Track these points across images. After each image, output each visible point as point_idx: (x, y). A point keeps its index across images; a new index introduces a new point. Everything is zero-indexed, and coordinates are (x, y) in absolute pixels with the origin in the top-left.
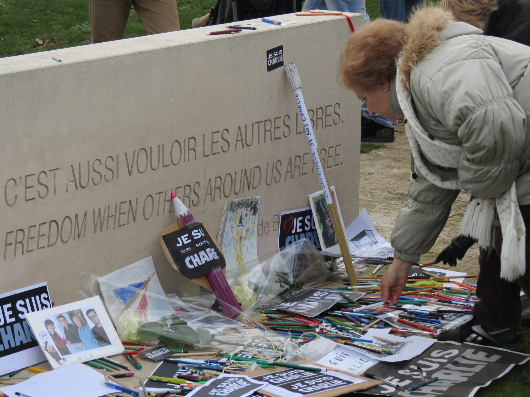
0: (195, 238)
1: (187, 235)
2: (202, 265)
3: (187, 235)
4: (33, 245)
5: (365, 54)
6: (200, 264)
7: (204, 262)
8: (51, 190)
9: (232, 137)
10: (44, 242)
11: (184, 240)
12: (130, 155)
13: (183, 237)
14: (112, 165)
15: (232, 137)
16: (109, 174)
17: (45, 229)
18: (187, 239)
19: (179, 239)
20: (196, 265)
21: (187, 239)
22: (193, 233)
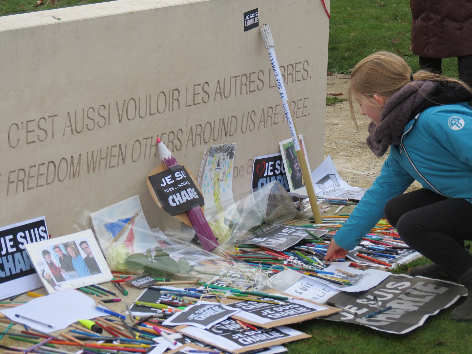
0: (177, 179)
1: (170, 176)
2: (184, 203)
3: (170, 176)
5: (189, 316)
6: (182, 202)
7: (185, 201)
11: (168, 181)
13: (166, 178)
18: (170, 179)
19: (163, 180)
20: (178, 203)
21: (170, 179)
22: (176, 175)
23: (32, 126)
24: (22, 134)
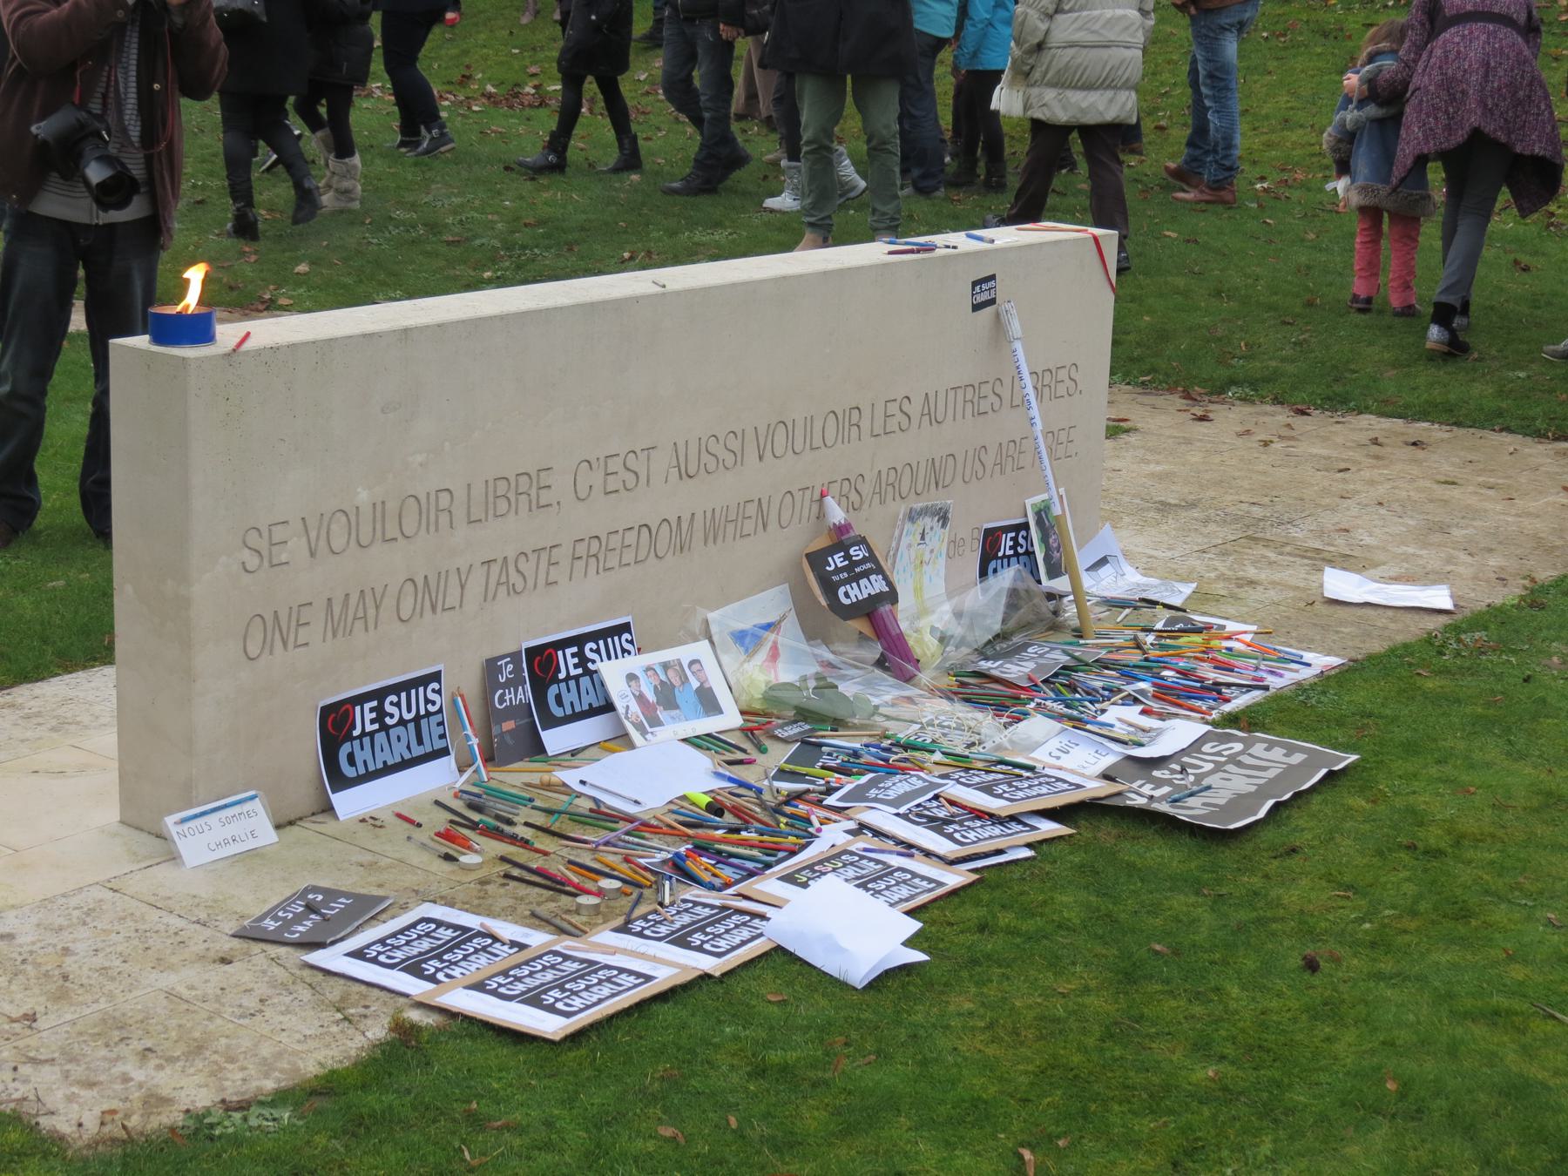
4: (613, 561)
8: (389, 603)
9: (914, 409)
10: (629, 556)
12: (762, 431)
14: (734, 444)
15: (914, 409)
16: (730, 459)
17: (631, 538)
23: (615, 464)
24: (597, 478)
